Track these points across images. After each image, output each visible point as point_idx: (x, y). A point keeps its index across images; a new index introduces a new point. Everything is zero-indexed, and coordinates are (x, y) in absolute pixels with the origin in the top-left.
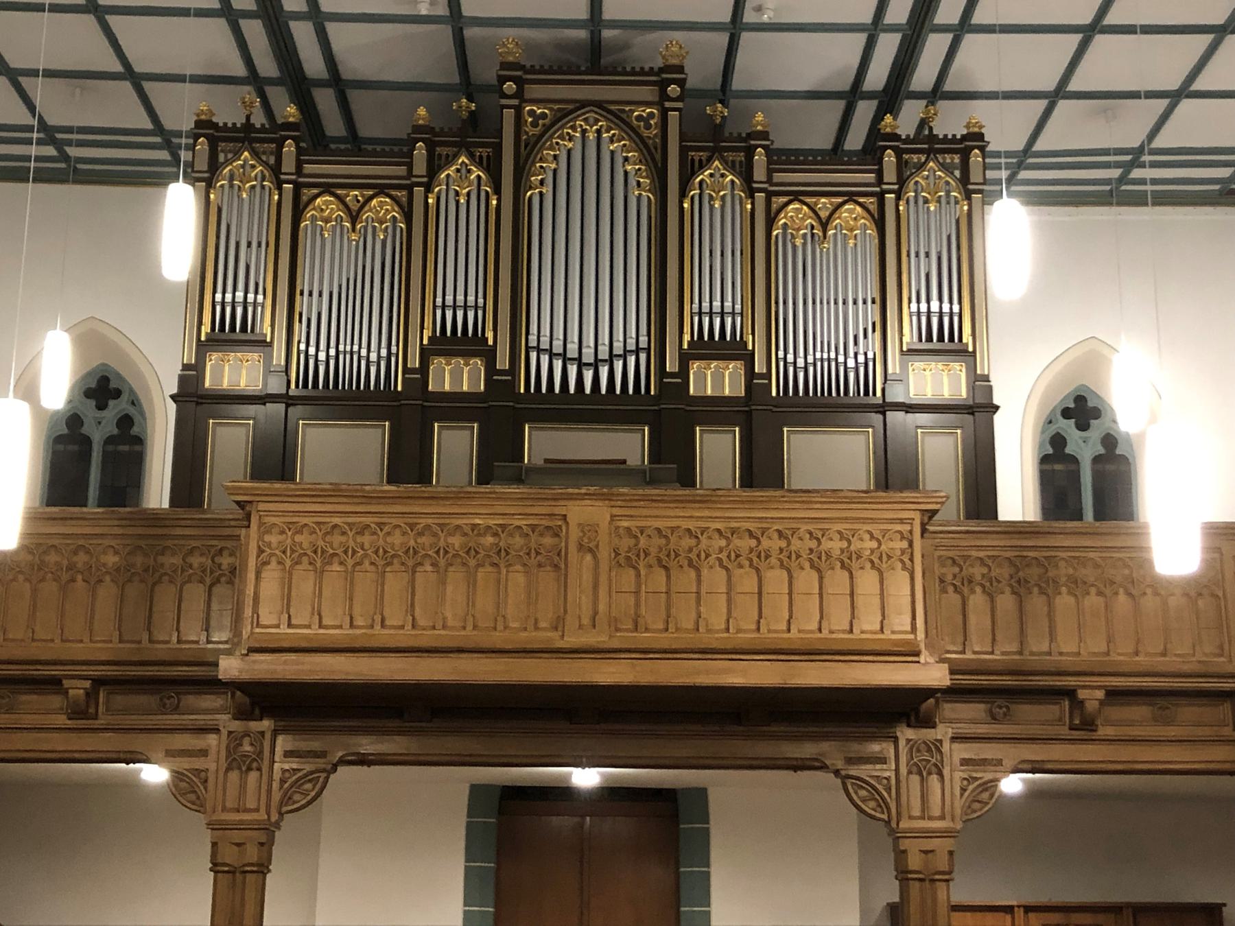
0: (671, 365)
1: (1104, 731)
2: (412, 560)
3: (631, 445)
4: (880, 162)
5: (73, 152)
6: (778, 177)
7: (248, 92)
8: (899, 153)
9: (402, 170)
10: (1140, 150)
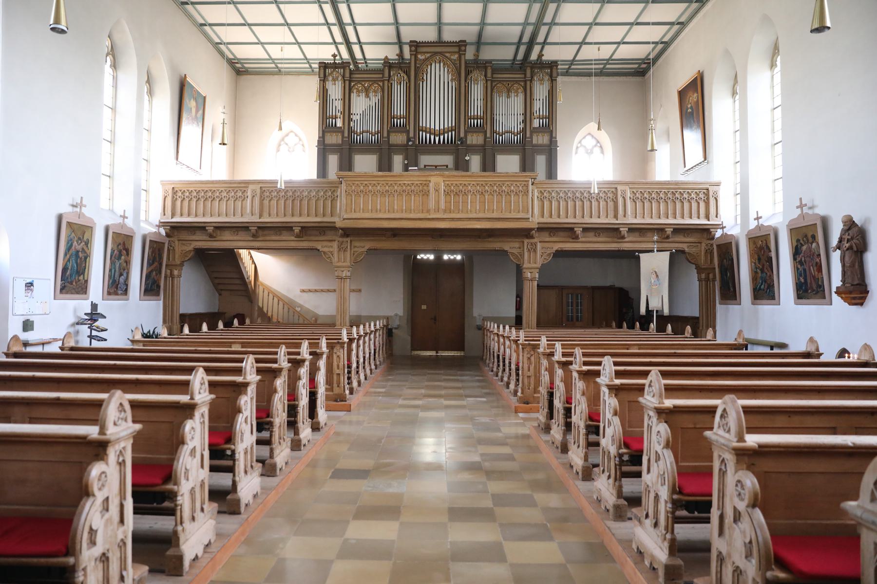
0: (462, 135)
1: (581, 240)
2: (383, 194)
3: (447, 160)
4: (525, 71)
5: (279, 65)
6: (495, 76)
7: (333, 47)
8: (532, 68)
9: (381, 76)
10: (608, 60)
